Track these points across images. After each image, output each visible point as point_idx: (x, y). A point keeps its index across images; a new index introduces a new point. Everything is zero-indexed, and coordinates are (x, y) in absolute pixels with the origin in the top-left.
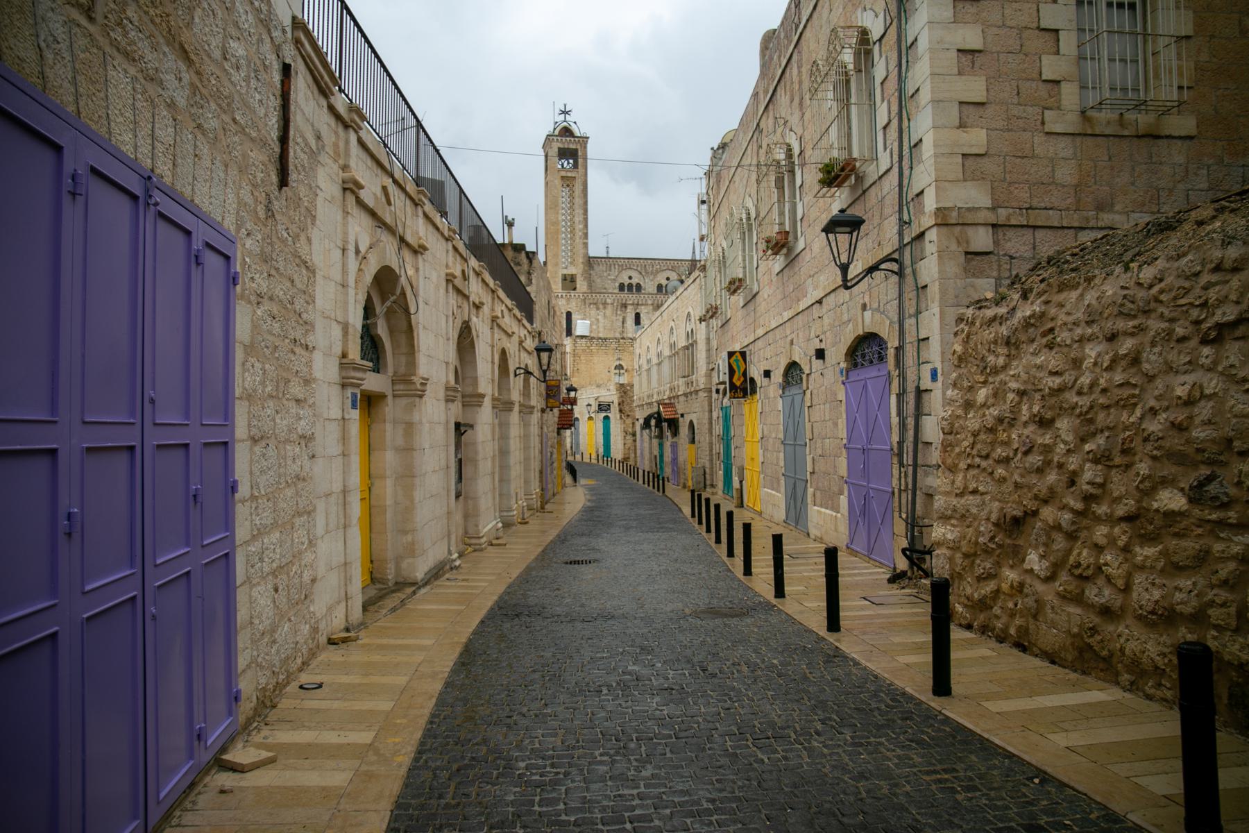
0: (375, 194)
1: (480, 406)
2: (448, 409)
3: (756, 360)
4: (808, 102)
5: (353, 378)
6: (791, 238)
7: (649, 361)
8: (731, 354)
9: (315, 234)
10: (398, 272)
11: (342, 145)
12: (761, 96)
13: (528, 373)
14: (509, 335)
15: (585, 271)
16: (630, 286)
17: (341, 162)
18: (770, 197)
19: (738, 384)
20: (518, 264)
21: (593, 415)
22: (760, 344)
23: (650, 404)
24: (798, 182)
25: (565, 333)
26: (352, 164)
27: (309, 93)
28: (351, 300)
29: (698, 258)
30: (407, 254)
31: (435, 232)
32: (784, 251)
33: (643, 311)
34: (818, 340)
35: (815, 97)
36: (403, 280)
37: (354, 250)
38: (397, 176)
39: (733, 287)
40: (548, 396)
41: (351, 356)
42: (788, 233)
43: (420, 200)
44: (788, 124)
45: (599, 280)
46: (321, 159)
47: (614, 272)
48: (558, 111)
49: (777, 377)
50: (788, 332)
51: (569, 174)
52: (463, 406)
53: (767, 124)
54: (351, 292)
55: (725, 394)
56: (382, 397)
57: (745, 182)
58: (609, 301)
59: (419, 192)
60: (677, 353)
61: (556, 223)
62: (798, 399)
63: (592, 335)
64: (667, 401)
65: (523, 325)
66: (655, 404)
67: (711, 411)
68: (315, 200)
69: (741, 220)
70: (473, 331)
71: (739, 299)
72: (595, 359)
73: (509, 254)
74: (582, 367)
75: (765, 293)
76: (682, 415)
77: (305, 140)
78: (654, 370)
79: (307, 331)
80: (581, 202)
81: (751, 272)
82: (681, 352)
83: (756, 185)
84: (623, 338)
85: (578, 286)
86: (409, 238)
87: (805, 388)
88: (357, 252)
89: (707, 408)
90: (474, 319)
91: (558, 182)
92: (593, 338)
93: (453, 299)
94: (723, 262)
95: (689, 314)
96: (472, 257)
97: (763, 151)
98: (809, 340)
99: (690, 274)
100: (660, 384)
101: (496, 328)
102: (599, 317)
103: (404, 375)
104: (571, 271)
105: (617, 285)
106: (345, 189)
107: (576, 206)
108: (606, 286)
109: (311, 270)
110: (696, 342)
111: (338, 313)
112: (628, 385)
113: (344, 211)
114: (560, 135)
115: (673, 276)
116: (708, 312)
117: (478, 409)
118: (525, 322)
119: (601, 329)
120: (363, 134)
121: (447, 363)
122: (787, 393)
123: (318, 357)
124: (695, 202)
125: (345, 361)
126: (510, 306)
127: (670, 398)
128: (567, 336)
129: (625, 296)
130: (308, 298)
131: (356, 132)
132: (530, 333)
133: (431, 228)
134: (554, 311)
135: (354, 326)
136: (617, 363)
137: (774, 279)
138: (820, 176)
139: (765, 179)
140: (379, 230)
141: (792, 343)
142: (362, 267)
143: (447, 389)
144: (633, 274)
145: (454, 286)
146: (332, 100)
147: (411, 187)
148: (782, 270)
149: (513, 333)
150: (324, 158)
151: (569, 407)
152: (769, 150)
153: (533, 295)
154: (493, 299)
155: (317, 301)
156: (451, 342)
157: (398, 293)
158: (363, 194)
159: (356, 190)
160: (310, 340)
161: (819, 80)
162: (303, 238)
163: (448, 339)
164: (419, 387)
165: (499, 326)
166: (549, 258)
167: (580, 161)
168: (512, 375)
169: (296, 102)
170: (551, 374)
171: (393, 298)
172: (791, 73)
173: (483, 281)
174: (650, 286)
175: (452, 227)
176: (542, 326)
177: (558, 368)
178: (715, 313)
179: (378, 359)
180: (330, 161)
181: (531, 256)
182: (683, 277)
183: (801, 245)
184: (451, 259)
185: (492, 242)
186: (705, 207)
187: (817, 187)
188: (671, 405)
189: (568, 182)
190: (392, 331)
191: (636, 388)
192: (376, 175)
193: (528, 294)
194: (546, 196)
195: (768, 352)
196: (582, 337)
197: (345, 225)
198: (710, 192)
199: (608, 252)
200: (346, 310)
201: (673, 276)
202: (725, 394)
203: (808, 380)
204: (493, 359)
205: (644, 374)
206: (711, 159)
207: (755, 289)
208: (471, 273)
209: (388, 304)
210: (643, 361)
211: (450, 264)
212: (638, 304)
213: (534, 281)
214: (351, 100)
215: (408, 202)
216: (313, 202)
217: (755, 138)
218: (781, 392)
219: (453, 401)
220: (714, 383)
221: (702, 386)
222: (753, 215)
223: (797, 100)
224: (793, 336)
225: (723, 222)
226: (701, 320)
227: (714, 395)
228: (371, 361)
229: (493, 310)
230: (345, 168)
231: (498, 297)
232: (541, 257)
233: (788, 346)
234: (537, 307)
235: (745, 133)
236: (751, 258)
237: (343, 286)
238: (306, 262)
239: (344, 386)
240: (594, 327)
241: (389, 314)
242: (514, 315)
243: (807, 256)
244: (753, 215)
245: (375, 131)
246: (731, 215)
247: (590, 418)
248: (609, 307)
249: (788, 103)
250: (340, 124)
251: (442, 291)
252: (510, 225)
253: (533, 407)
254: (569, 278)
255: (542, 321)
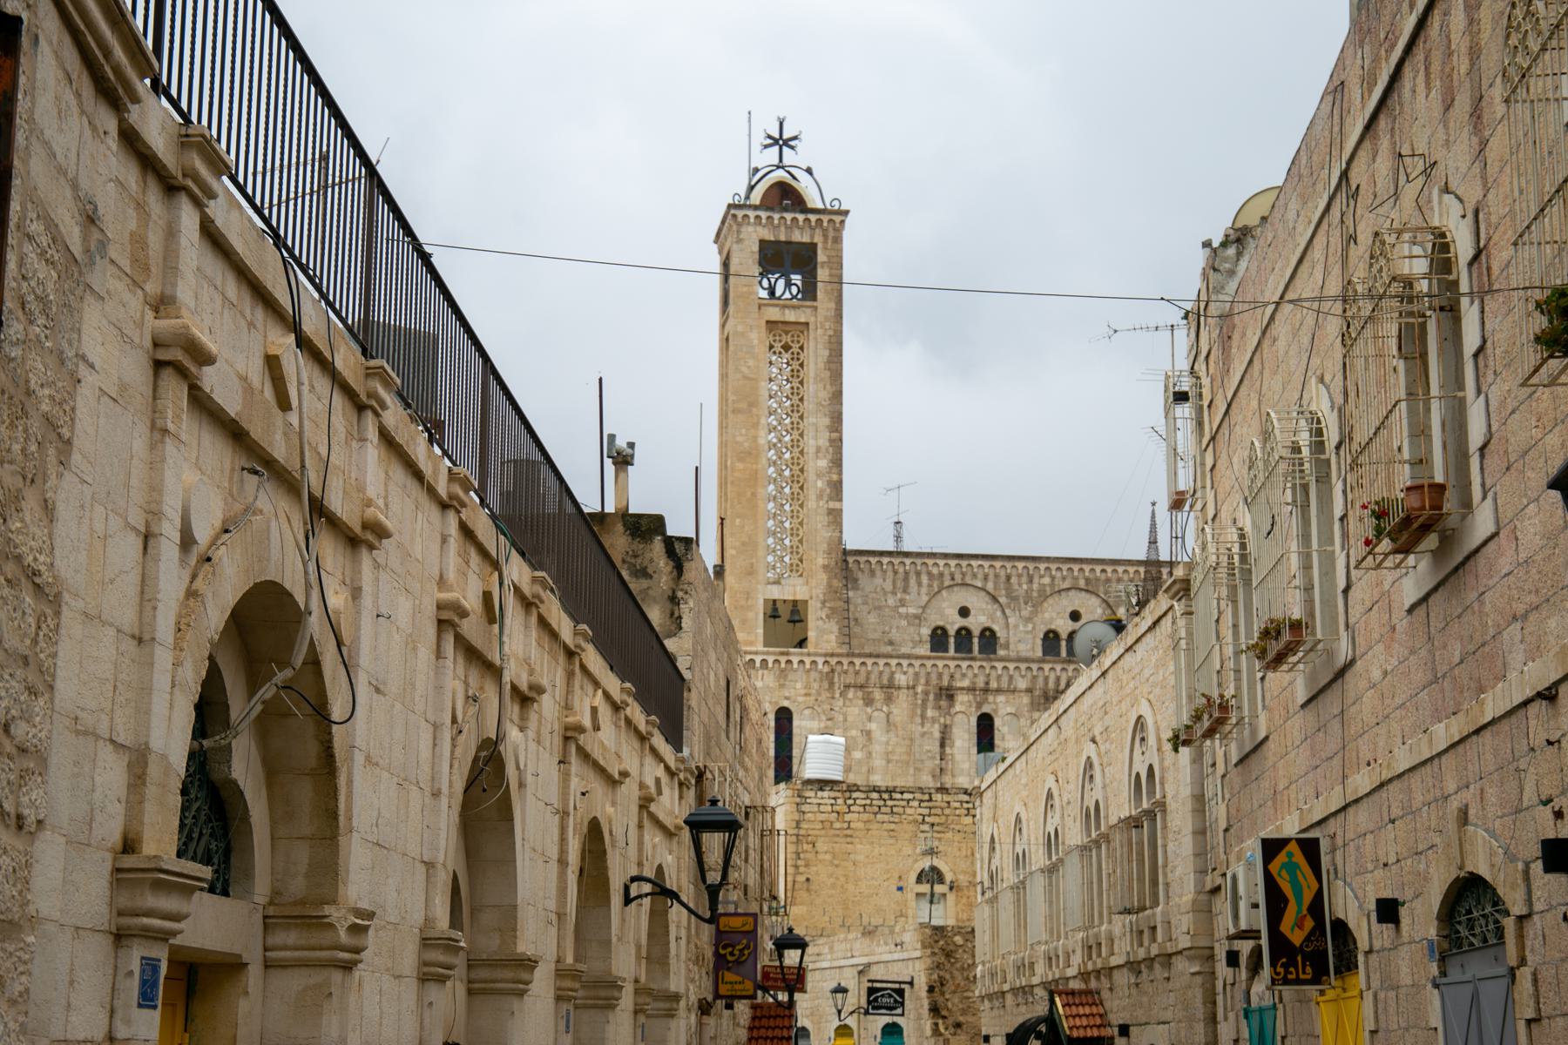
0: (244, 379)
1: (521, 994)
2: (424, 1005)
3: (1351, 867)
4: (1500, 109)
5: (149, 913)
6: (1450, 504)
7: (1020, 860)
8: (1271, 848)
9: (67, 493)
10: (300, 599)
11: (155, 240)
12: (1355, 92)
13: (663, 893)
14: (612, 782)
15: (831, 591)
16: (964, 635)
17: (152, 287)
18: (1382, 383)
19: (1297, 938)
20: (643, 573)
21: (851, 1022)
22: (1361, 818)
23: (1025, 991)
24: (1471, 341)
25: (771, 773)
26: (184, 292)
27: (69, 97)
28: (162, 680)
29: (1164, 556)
30: (328, 548)
31: (411, 484)
32: (1432, 541)
33: (1002, 708)
34: (1547, 812)
35: (1521, 92)
36: (315, 624)
37: (176, 537)
38: (308, 327)
39: (1274, 647)
40: (721, 963)
41: (149, 848)
42: (1441, 488)
43: (372, 395)
44: (1438, 173)
45: (872, 619)
46: (95, 279)
47: (917, 596)
48: (759, 139)
49: (1421, 920)
50: (1451, 786)
51: (791, 316)
52: (470, 992)
53: (1374, 171)
54: (163, 657)
55: (1255, 967)
56: (232, 967)
57: (1306, 341)
58: (901, 679)
59: (370, 373)
60: (1106, 838)
61: (751, 454)
62: (1492, 993)
63: (852, 778)
64: (1075, 985)
65: (653, 750)
66: (1041, 993)
67: (1212, 1020)
68: (72, 395)
69: (1296, 449)
70: (511, 771)
71: (1292, 682)
72: (861, 850)
73: (618, 543)
74: (821, 873)
75: (1372, 666)
76: (1124, 1030)
77: (51, 226)
78: (1038, 886)
79: (24, 775)
80: (824, 395)
81: (1328, 603)
82: (1117, 838)
83: (1339, 351)
84: (942, 790)
85: (811, 634)
86: (336, 502)
87: (1512, 960)
88: (187, 541)
89: (1200, 1011)
90: (513, 734)
91: (758, 337)
92: (853, 788)
93: (455, 676)
94: (1241, 570)
95: (1140, 722)
96: (515, 557)
97: (1359, 252)
98: (1518, 811)
99: (1142, 604)
100: (1054, 933)
101: (646, 823)
102: (873, 726)
103: (302, 902)
104: (793, 589)
105: (926, 632)
106: (158, 365)
107: (808, 406)
108: (895, 635)
109: (48, 595)
110: (1162, 805)
111: (119, 721)
112: (958, 930)
113: (153, 427)
114: (766, 204)
115: (1092, 608)
116: (1197, 717)
117: (515, 1003)
118: (659, 741)
119: (878, 762)
120: (216, 210)
121: (429, 865)
122: (1455, 974)
123: (50, 853)
124: (1156, 398)
125: (129, 861)
126: (617, 695)
127: (1084, 975)
128: (777, 781)
129: (949, 666)
130: (32, 677)
131: (198, 203)
132: (671, 773)
133: (399, 474)
134: (744, 709)
135: (164, 757)
136: (926, 863)
137: (1402, 624)
138: (1540, 322)
139: (1368, 332)
140: (253, 480)
141: (1463, 817)
142: (199, 584)
143: (426, 942)
144: (975, 601)
145: (459, 639)
146: (134, 115)
147: (347, 358)
148: (1425, 599)
149: (625, 774)
150: (103, 278)
151: (783, 997)
152: (1379, 249)
153: (682, 664)
154: (570, 675)
155: (59, 685)
156: (444, 801)
157: (298, 660)
158: (213, 380)
159: (193, 368)
160: (32, 800)
161: (1534, 45)
162: (31, 504)
163: (436, 794)
164: (343, 937)
165: (584, 755)
166: (729, 552)
167: (822, 274)
168: (616, 899)
169: (31, 120)
170: (731, 898)
171: (281, 676)
172: (1445, 28)
173: (543, 622)
174: (1021, 638)
175: (462, 470)
176: (708, 754)
177: (752, 878)
178: (1221, 721)
179: (227, 852)
180: (118, 286)
181: (680, 551)
182: (1121, 612)
183: (1482, 523)
184: (453, 561)
185: (570, 509)
186: (1184, 411)
187: (1532, 356)
188: (1088, 997)
189: (787, 338)
190: (272, 771)
191: (982, 941)
192: (251, 325)
193: (671, 659)
194: (724, 377)
195: (1390, 844)
196: (822, 784)
197: (155, 464)
198: (1201, 367)
199: (898, 538)
200: (143, 712)
201: (1092, 608)
202: (1255, 967)
203: (1521, 937)
204: (563, 851)
205: (1007, 900)
206: (1205, 275)
207: (1343, 651)
208: (511, 602)
209: (267, 691)
210: (1004, 860)
211: (451, 575)
212: (986, 690)
213: (687, 622)
214: (186, 116)
215: (338, 400)
216: (65, 402)
217: (1336, 212)
218: (1434, 969)
219: (442, 980)
220: (1220, 933)
221: (1184, 942)
222: (1332, 436)
223: (1463, 103)
224: (1468, 796)
225: (1240, 457)
226: (1177, 742)
227: (1222, 970)
228: (207, 861)
229: (568, 707)
230: (162, 304)
231: (583, 668)
232: (708, 553)
233: (1452, 826)
234: (693, 699)
235: (1304, 200)
236: (1328, 560)
237: (140, 641)
238: (37, 573)
239: (120, 937)
240: (858, 755)
241: (269, 722)
242: (628, 722)
243: (1503, 558)
244: (1332, 436)
245: (251, 200)
246: (1266, 435)
247: (843, 1031)
248: (903, 698)
249: (1437, 107)
250: (153, 184)
251: (425, 653)
252: (623, 460)
253: (676, 997)
254: (784, 612)
255: (708, 737)
